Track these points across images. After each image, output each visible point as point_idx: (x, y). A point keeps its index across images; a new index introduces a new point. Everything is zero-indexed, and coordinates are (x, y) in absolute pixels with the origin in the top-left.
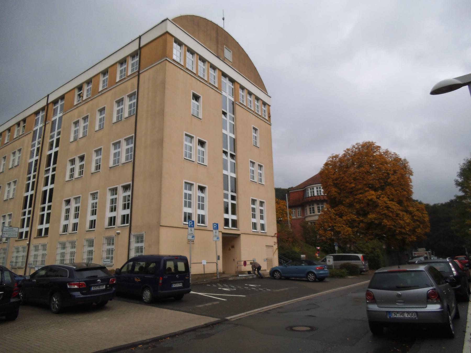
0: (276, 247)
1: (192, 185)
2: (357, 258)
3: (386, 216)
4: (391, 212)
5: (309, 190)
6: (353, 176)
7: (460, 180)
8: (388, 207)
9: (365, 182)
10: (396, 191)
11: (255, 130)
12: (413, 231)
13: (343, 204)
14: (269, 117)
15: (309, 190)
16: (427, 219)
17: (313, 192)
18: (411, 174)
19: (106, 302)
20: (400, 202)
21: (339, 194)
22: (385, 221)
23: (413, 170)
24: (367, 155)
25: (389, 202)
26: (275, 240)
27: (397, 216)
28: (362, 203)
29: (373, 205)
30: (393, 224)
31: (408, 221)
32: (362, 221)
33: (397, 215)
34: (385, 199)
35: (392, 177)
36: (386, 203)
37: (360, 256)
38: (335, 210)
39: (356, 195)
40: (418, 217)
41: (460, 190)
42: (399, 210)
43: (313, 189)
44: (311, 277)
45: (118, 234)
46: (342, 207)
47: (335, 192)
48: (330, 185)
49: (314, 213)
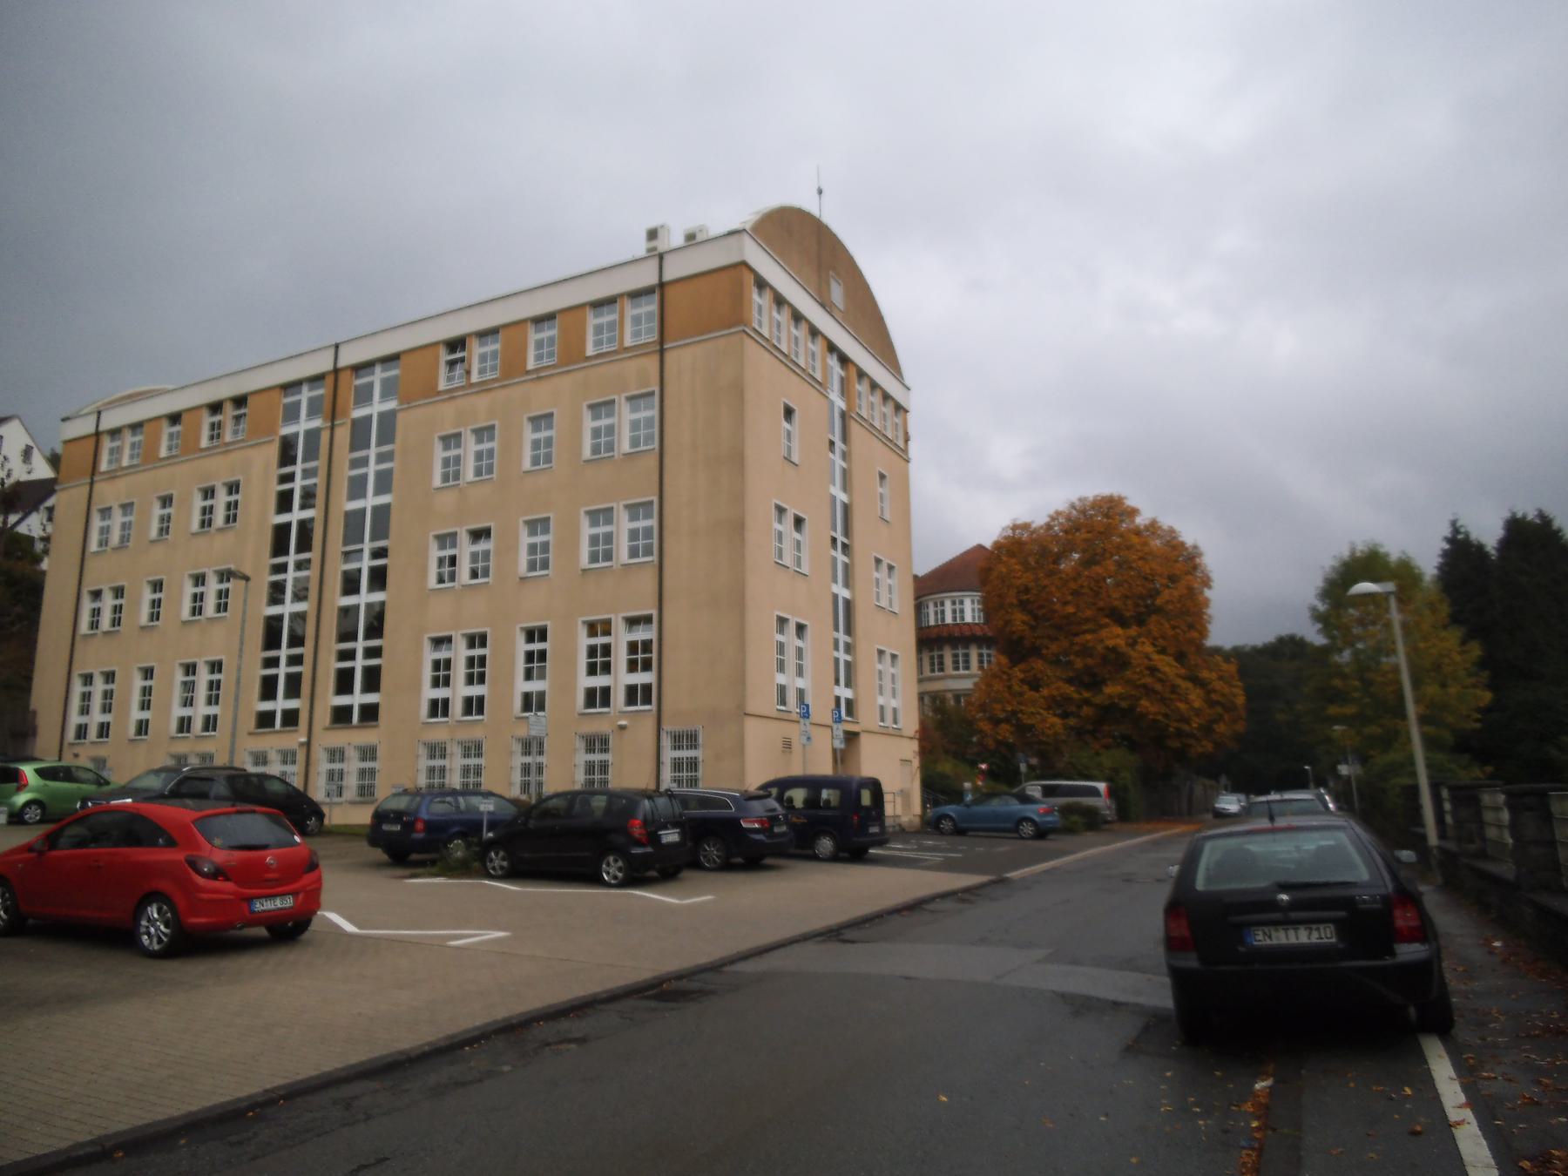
0: (916, 763)
1: (454, 535)
2: (1094, 792)
3: (1148, 691)
4: (1160, 680)
5: (931, 605)
6: (1073, 585)
7: (1322, 607)
8: (1153, 670)
9: (1101, 604)
10: (1174, 628)
11: (882, 477)
12: (1207, 730)
13: (1041, 656)
14: (907, 440)
15: (931, 605)
16: (1240, 700)
17: (943, 612)
18: (1207, 582)
19: (763, 857)
20: (1180, 657)
21: (1032, 628)
22: (1144, 703)
23: (1214, 576)
24: (1106, 532)
25: (1155, 657)
26: (915, 746)
27: (1173, 692)
28: (1091, 656)
29: (1117, 661)
30: (1164, 709)
31: (1197, 704)
32: (1087, 702)
33: (1174, 689)
34: (1149, 649)
35: (1166, 595)
36: (1150, 660)
37: (1102, 786)
38: (1022, 671)
39: (1076, 635)
40: (1223, 695)
41: (1319, 631)
42: (1178, 676)
43: (942, 604)
44: (1028, 829)
45: (622, 728)
46: (1039, 665)
47: (1023, 622)
48: (1011, 605)
49: (941, 670)
